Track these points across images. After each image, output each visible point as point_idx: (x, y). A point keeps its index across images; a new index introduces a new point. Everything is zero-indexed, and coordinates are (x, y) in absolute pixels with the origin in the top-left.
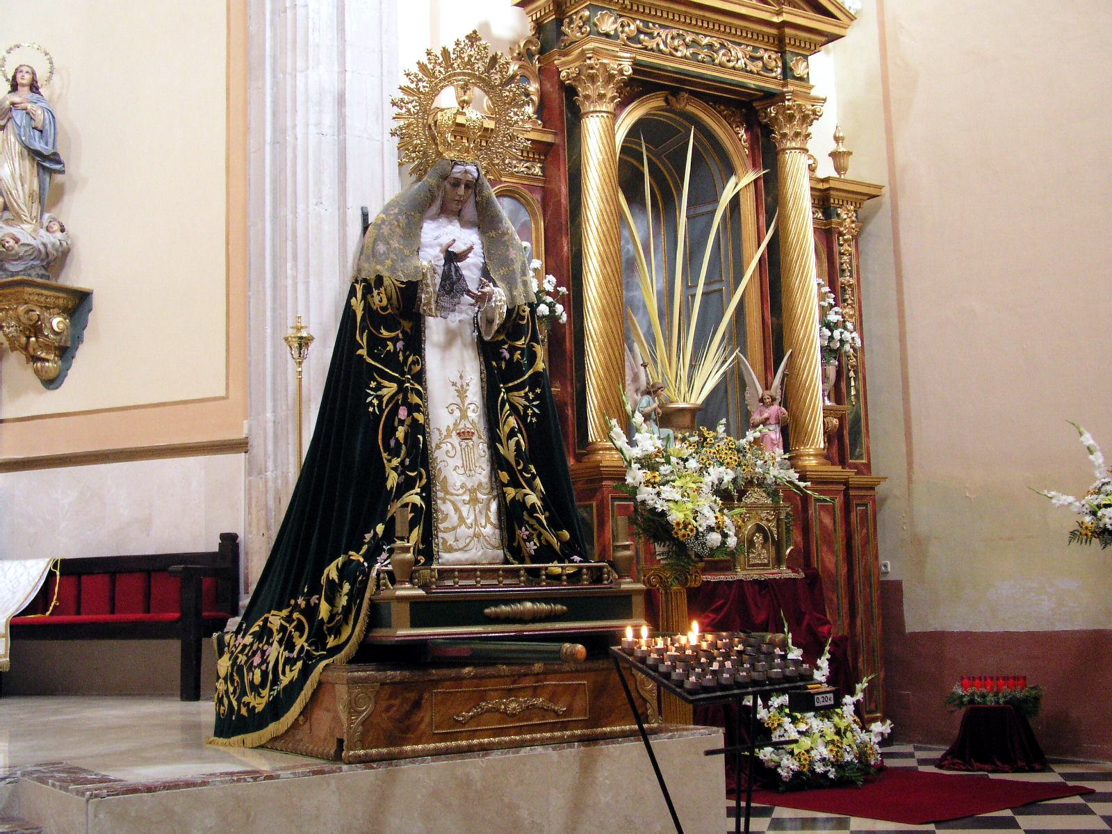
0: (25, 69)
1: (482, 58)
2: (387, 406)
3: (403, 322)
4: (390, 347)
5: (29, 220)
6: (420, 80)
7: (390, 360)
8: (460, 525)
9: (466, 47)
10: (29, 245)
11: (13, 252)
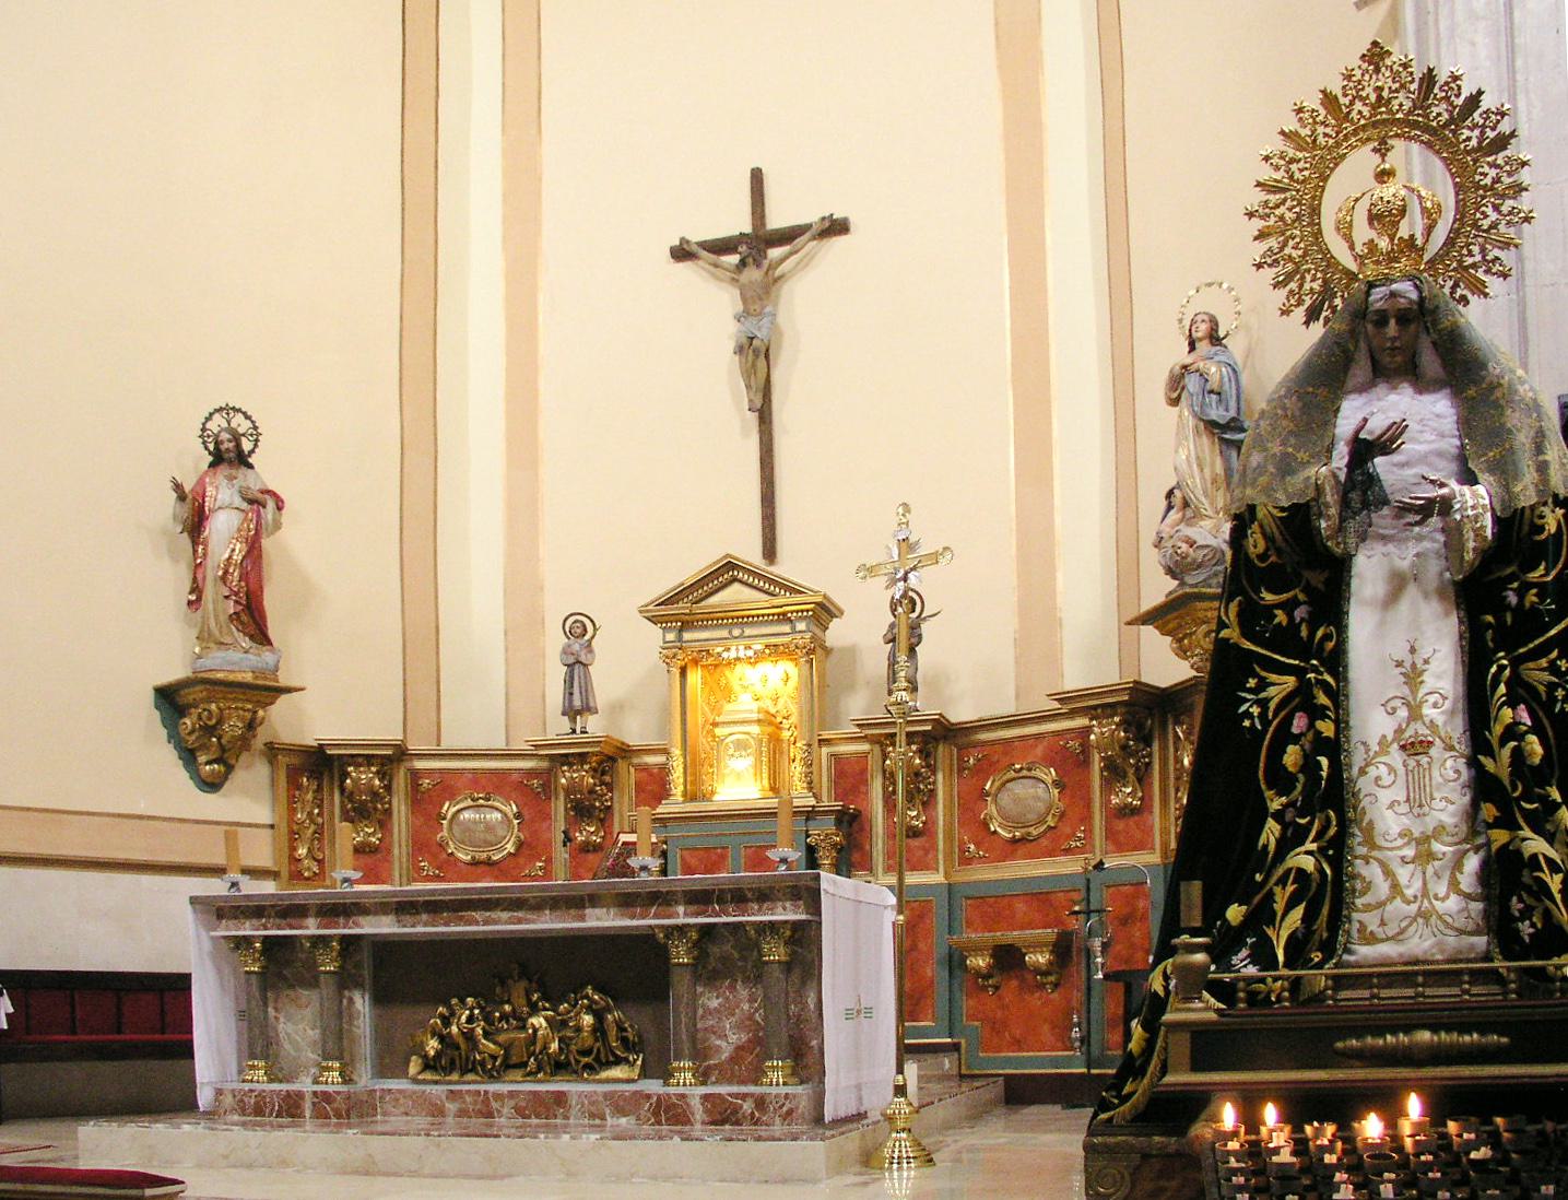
0: (1199, 318)
1: (1403, 86)
2: (1275, 717)
3: (1307, 574)
4: (1281, 617)
5: (1210, 513)
6: (1293, 161)
7: (1285, 640)
8: (1391, 898)
9: (1367, 77)
10: (1207, 546)
11: (1189, 559)
